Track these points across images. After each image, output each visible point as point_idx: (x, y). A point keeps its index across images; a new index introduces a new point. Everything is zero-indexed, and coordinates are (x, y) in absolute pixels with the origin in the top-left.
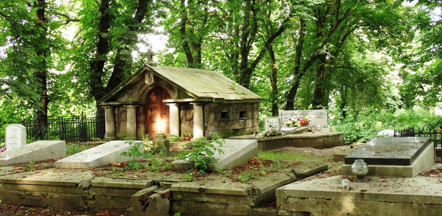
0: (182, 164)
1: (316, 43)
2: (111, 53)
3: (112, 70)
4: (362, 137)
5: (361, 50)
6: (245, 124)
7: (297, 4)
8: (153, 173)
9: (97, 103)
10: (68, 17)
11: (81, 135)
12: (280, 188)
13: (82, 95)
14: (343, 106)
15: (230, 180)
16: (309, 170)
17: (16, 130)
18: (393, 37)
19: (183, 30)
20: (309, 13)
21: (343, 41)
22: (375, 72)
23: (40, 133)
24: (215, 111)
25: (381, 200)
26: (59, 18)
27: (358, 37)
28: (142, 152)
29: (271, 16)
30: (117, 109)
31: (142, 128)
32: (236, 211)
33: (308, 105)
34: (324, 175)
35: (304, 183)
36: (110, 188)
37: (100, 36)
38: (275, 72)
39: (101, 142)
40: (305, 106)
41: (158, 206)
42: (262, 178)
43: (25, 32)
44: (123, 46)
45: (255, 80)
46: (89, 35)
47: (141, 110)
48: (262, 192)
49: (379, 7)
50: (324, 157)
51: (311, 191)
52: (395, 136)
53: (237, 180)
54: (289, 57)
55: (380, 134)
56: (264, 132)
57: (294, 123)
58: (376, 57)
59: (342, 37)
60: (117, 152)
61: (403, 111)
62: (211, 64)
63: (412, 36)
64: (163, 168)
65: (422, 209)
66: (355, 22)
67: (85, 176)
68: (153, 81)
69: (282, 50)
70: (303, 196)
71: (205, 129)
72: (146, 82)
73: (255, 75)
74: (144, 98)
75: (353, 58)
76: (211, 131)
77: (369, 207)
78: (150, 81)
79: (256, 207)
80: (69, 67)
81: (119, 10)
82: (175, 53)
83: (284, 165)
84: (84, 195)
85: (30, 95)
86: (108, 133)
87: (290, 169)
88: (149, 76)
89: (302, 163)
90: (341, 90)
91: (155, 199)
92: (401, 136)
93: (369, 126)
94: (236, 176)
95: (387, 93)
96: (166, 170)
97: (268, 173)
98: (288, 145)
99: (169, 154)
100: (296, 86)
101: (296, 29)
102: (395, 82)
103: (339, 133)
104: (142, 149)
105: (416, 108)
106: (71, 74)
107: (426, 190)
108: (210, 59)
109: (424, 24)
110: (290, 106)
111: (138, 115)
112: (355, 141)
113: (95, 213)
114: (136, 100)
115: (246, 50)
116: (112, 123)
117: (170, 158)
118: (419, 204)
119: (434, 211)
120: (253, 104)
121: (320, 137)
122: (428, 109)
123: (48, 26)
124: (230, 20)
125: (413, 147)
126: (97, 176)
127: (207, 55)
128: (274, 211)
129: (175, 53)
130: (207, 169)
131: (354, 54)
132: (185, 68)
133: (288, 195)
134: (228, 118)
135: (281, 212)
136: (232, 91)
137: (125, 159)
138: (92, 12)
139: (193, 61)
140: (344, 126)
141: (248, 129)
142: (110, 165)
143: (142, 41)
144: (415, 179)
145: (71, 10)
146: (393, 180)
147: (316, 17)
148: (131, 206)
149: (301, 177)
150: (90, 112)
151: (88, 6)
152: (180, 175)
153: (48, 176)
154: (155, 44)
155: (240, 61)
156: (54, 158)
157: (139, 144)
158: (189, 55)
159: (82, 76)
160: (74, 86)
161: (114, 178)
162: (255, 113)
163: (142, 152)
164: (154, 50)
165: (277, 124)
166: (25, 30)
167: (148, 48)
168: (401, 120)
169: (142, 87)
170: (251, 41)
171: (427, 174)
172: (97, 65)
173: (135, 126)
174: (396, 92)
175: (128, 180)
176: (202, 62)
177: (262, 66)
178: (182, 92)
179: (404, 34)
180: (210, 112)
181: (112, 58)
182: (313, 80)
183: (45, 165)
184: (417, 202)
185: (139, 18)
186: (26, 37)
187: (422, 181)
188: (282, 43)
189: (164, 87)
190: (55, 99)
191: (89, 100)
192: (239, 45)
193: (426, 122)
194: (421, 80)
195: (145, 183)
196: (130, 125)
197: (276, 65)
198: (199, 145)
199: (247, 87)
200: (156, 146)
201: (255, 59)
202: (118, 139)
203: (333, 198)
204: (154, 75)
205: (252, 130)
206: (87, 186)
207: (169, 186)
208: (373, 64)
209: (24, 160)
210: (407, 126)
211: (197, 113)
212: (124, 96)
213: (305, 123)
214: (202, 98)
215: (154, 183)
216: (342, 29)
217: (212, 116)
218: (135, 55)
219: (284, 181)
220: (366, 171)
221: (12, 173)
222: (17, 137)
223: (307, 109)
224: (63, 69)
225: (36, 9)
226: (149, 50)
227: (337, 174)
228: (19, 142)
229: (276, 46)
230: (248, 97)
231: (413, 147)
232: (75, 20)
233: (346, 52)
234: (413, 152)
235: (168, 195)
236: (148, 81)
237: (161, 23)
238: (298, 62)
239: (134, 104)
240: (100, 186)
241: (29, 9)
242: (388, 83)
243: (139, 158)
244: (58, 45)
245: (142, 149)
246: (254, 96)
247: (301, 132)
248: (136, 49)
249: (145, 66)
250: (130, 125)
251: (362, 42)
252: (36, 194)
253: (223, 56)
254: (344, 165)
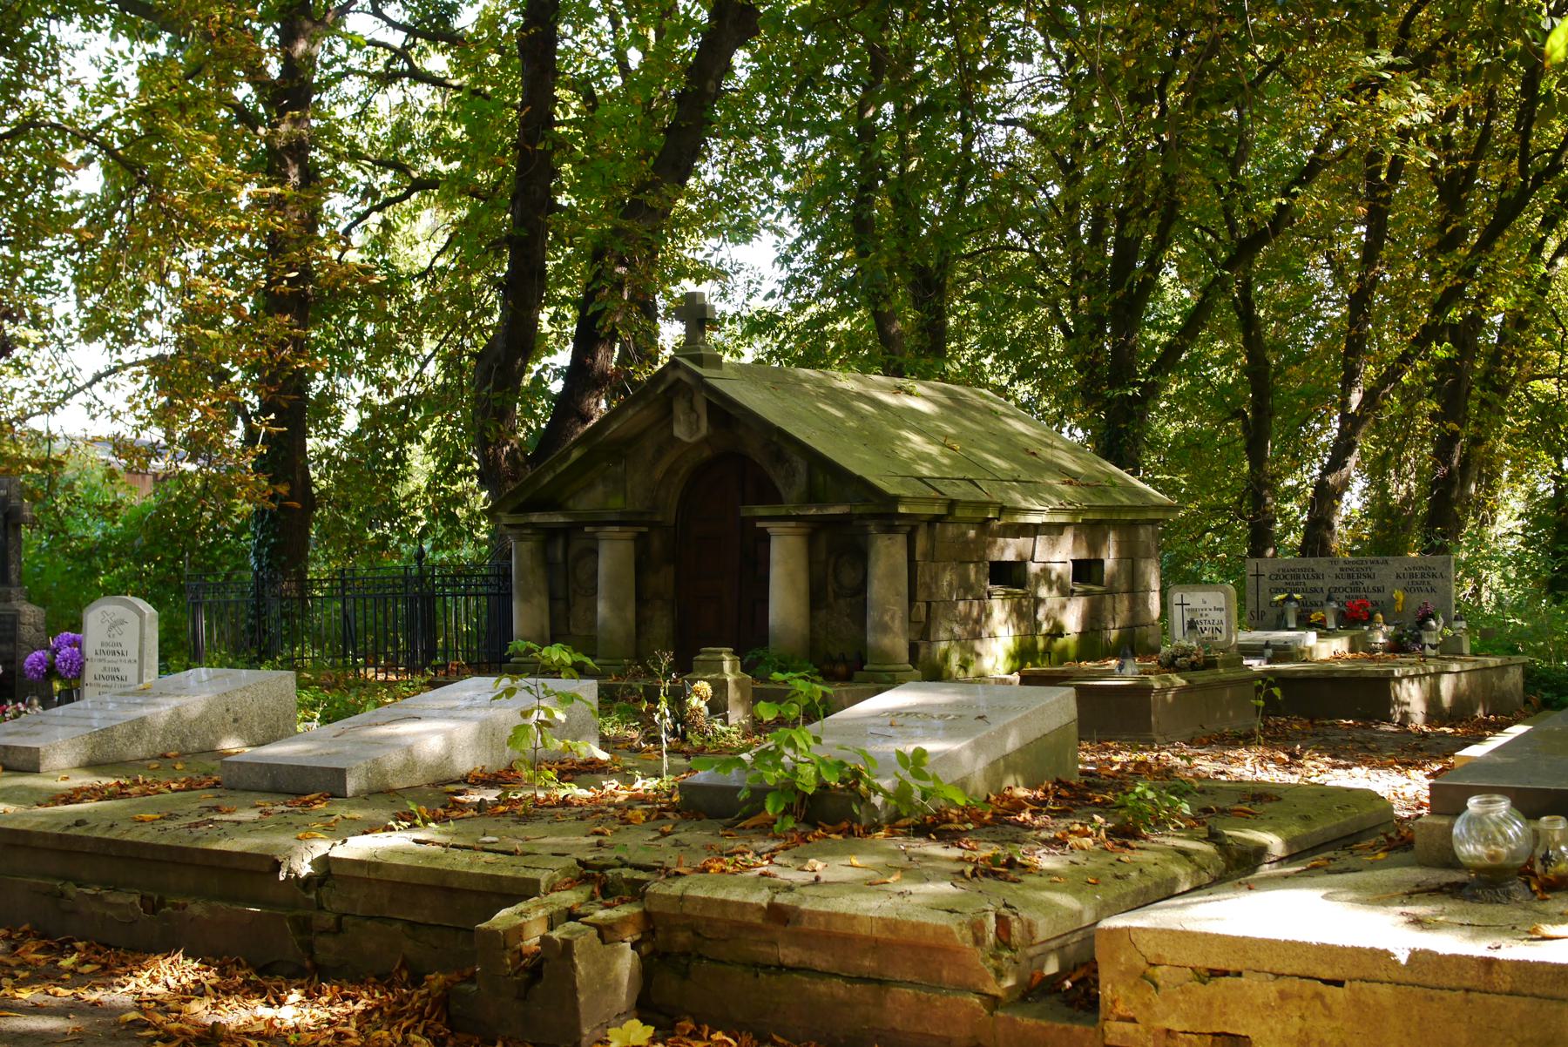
17: (122, 622)
30: (560, 543)
70: (1222, 965)
72: (680, 431)
77: (1521, 1026)
78: (693, 427)
84: (300, 912)
88: (692, 408)
116: (541, 601)
135: (1115, 1030)
139: (912, 348)
165: (1221, 616)
204: (709, 404)
212: (591, 485)
222: (124, 648)
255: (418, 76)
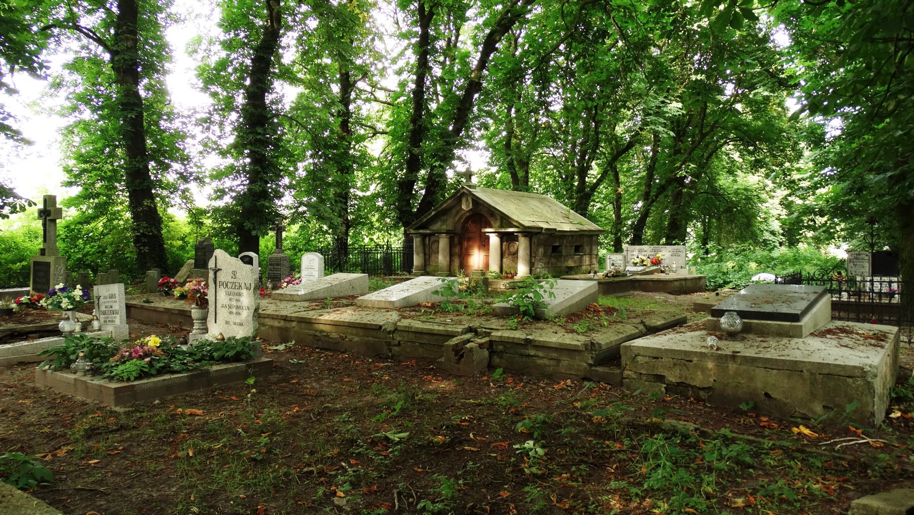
0: (505, 308)
1: (673, 162)
2: (423, 172)
3: (423, 192)
4: (731, 282)
5: (731, 172)
6: (581, 260)
7: (650, 115)
8: (469, 318)
9: (405, 231)
10: (375, 129)
11: (386, 268)
12: (627, 344)
13: (388, 220)
14: (705, 243)
15: (563, 330)
16: (663, 322)
18: (774, 156)
19: (508, 145)
20: (665, 125)
21: (707, 159)
22: (748, 199)
23: (340, 263)
24: (545, 244)
25: (760, 365)
26: (365, 130)
27: (727, 155)
28: (457, 292)
29: (617, 128)
31: (457, 263)
32: (570, 369)
33: (660, 238)
34: (682, 329)
35: (657, 338)
36: (419, 333)
37: (410, 152)
38: (619, 196)
39: (408, 277)
40: (656, 241)
41: (475, 357)
42: (603, 330)
43: (327, 146)
44: (437, 164)
45: (595, 207)
46: (399, 150)
47: (456, 240)
48: (604, 348)
49: (755, 119)
50: (681, 305)
51: (666, 350)
52: (776, 282)
53: (573, 331)
54: (638, 179)
55: (755, 278)
56: (605, 272)
57: (643, 261)
58: (752, 180)
59: (706, 155)
60: (427, 290)
61: (784, 249)
62: (540, 186)
63: (799, 155)
64: (482, 311)
65: (815, 379)
66: (725, 136)
67: (390, 318)
68: (471, 206)
69: (629, 170)
70: (656, 355)
71: (531, 265)
72: (464, 207)
73: (594, 201)
74: (459, 226)
75: (721, 182)
76: (540, 268)
78: (468, 206)
79: (596, 366)
80: (374, 188)
81: (433, 121)
82: (497, 172)
83: (632, 314)
85: (330, 219)
86: (417, 267)
87: (638, 320)
89: (654, 312)
90: (703, 223)
91: (471, 349)
92: (785, 283)
93: (741, 268)
94: (570, 326)
95: (763, 227)
96: (485, 314)
97: (610, 323)
98: (635, 289)
99: (488, 294)
100: (645, 214)
101: (647, 145)
102: (775, 212)
103: (700, 275)
104: (456, 288)
105: (802, 246)
106: (375, 196)
107: (822, 356)
108: (540, 180)
109: (816, 138)
110: (637, 240)
111: (451, 245)
112: (721, 286)
113: (400, 362)
114: (240, 333)
115: (583, 171)
116: (422, 255)
117: (489, 300)
118: (812, 374)
119: (832, 384)
120: (591, 236)
121: (676, 280)
122: (818, 248)
123: (352, 139)
124: (566, 133)
125: (802, 299)
126: (404, 317)
127: (536, 175)
128: (618, 371)
129: (497, 172)
130: (535, 315)
131: (721, 177)
132: (510, 191)
133: (636, 352)
134: (561, 252)
136: (567, 221)
137: (437, 298)
138: (403, 123)
139: (520, 183)
140: (708, 267)
141: (584, 267)
142: (419, 305)
143: (460, 158)
144: (806, 340)
145: (378, 121)
146: (775, 340)
147: (673, 130)
148: (442, 356)
149: (652, 330)
150: (396, 241)
151: (398, 116)
152: (502, 322)
153: (347, 315)
154: (475, 161)
155: (576, 184)
156: (355, 293)
157: (453, 282)
158: (514, 175)
159: (389, 197)
160: (379, 209)
161: (423, 322)
162: (594, 247)
163: (457, 292)
164: (474, 169)
166: (326, 143)
167: (466, 166)
168: (783, 261)
169: (457, 213)
170: (591, 159)
171: (823, 334)
172: (407, 186)
173: (448, 259)
174: (776, 226)
175: (439, 324)
176: (530, 184)
177: (604, 189)
178: (505, 220)
179: (789, 151)
180: (538, 245)
181: (423, 178)
182: (666, 208)
183: (345, 301)
184: (808, 370)
185: (457, 131)
186: (327, 152)
187: (815, 343)
188: (629, 162)
189: (483, 215)
190: (357, 225)
191: (395, 227)
192: (576, 164)
193: (816, 265)
194: (808, 211)
195: (459, 329)
196: (442, 259)
197: (621, 190)
198: (524, 286)
199: (584, 215)
200: (473, 284)
201: (595, 181)
202: (427, 274)
203: (695, 359)
205: (589, 268)
206: (392, 329)
207: (488, 334)
208: (746, 190)
209: (321, 295)
210: (792, 270)
211: (522, 245)
213: (657, 262)
214: (529, 227)
215: (470, 330)
216: (707, 146)
217: (541, 250)
218: (450, 173)
219: (631, 335)
220: (739, 327)
221: (308, 309)
223: (658, 244)
224: (368, 190)
225: (340, 120)
226: (468, 169)
227: (701, 330)
228: (316, 274)
229: (622, 165)
230: (585, 228)
231: (802, 299)
232: (384, 133)
233: (711, 173)
234: (803, 305)
235: (486, 345)
236: (466, 206)
237: (482, 137)
238: (649, 186)
239: (447, 232)
240: (407, 330)
241: (331, 119)
242: (765, 213)
243: (452, 299)
244: (363, 161)
245: (456, 288)
246: (593, 226)
247: (651, 273)
248: (452, 167)
249: (463, 188)
250: (442, 259)
251: (733, 161)
252: (334, 335)
253: (555, 177)
254: (710, 318)
255: (376, 100)
